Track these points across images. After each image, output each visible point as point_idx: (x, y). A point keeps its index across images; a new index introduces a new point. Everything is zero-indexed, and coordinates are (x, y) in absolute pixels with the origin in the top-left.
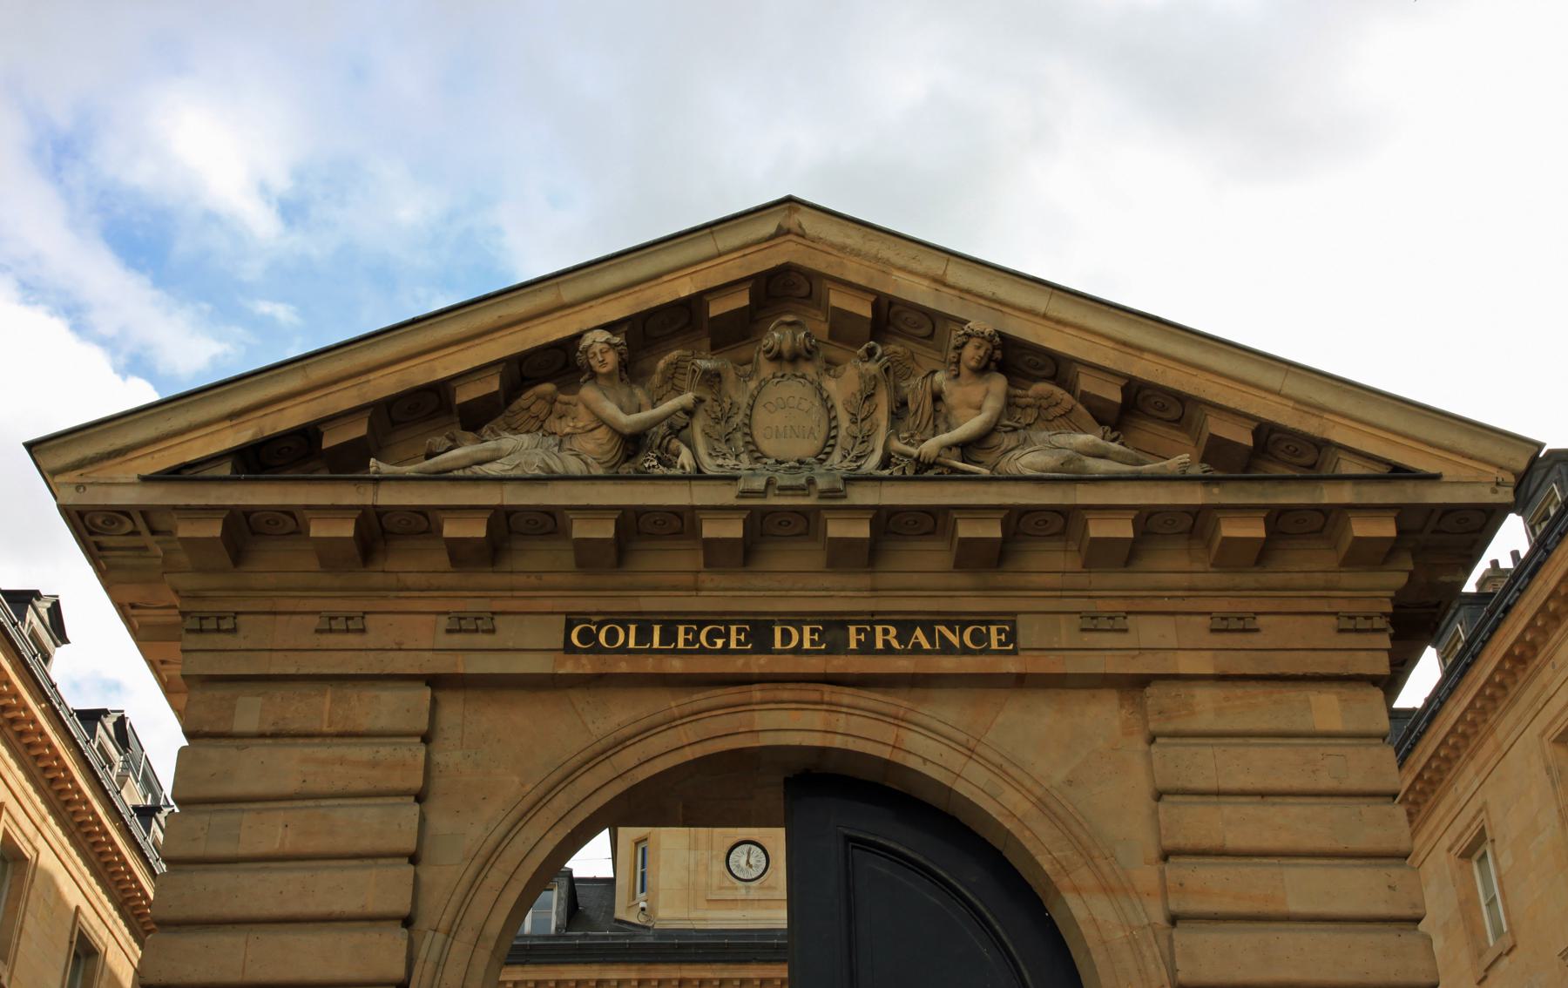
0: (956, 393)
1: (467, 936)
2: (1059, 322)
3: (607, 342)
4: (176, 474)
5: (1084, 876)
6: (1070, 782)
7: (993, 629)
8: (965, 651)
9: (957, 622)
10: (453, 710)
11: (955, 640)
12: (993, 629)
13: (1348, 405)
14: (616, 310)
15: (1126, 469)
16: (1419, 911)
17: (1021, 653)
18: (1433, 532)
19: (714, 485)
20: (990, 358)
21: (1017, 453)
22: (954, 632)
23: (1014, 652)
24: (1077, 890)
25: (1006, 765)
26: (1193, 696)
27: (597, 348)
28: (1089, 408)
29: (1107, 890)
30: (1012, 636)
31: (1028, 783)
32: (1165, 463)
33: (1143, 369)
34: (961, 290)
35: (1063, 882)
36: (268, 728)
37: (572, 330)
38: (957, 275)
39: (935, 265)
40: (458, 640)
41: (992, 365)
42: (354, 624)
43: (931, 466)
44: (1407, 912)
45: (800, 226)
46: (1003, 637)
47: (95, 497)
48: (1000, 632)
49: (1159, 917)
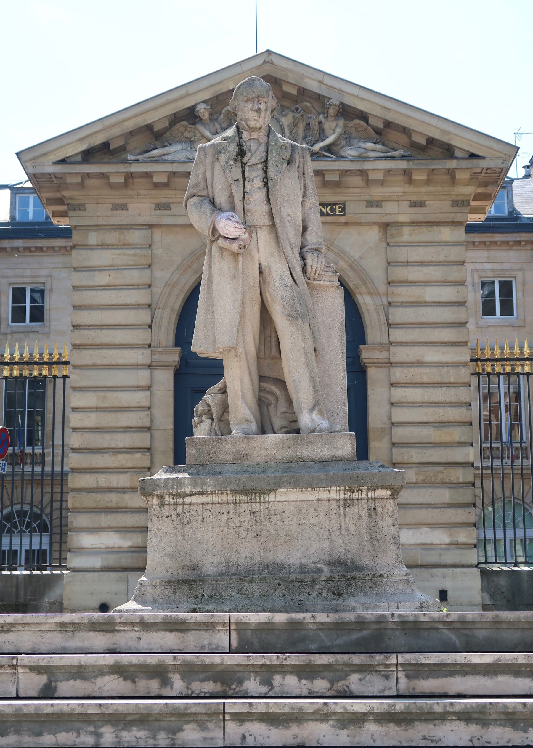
0: (329, 125)
1: (168, 310)
2: (362, 99)
3: (205, 108)
4: (63, 161)
5: (363, 289)
6: (361, 258)
7: (337, 207)
8: (328, 215)
9: (325, 204)
10: (158, 234)
11: (324, 211)
12: (337, 207)
13: (458, 132)
14: (206, 96)
15: (382, 155)
16: (466, 299)
17: (346, 215)
18: (486, 173)
19: (67, 745)
20: (338, 112)
21: (346, 148)
22: (324, 208)
23: (344, 215)
24: (361, 294)
25: (340, 253)
26: (402, 229)
27: (202, 111)
28: (372, 128)
29: (370, 293)
30: (344, 209)
31: (347, 259)
32: (395, 152)
33: (390, 117)
34: (329, 86)
35: (356, 291)
36: (100, 243)
37: (192, 104)
38: (327, 81)
39: (320, 77)
40: (158, 212)
41: (339, 114)
42: (124, 207)
43: (317, 153)
44: (462, 300)
45: (272, 60)
46: (340, 209)
47: (40, 170)
48: (339, 208)
49: (385, 302)
